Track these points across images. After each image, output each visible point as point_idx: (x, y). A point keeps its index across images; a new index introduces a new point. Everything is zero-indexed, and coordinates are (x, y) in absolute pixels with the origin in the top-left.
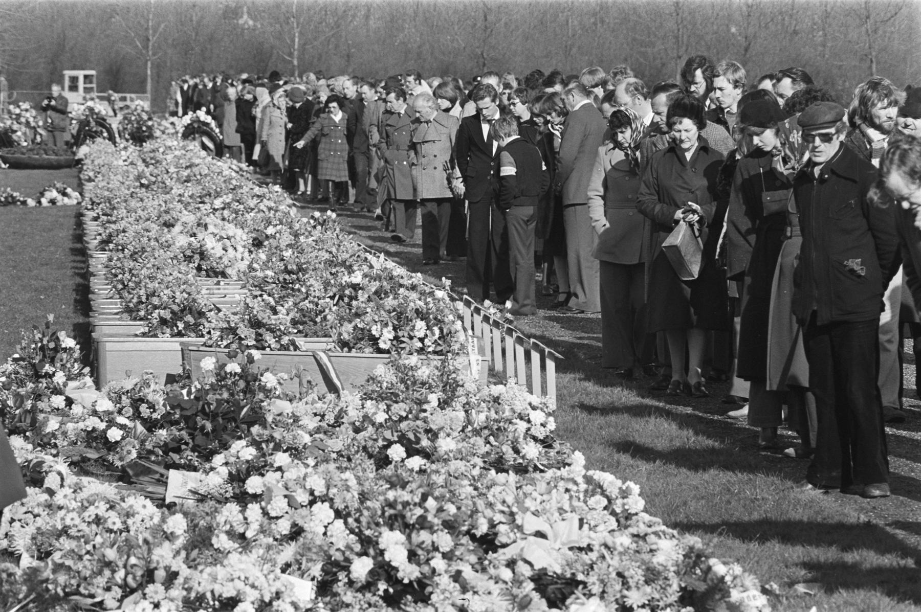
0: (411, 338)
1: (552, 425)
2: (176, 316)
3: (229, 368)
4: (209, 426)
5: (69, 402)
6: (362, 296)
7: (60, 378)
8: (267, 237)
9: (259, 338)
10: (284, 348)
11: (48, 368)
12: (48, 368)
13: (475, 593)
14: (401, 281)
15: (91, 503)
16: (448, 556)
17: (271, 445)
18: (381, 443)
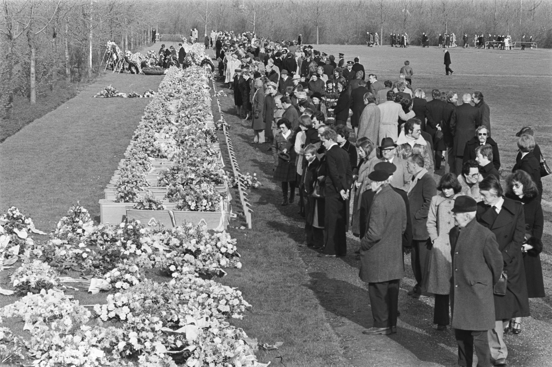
0: (202, 206)
1: (235, 248)
2: (126, 195)
3: (129, 227)
4: (109, 260)
5: (84, 231)
6: (194, 182)
7: (81, 223)
8: (186, 140)
9: (150, 206)
10: (159, 209)
11: (77, 219)
12: (77, 219)
13: (151, 362)
14: (212, 173)
15: (49, 306)
16: (152, 341)
17: (124, 271)
18: (168, 264)
